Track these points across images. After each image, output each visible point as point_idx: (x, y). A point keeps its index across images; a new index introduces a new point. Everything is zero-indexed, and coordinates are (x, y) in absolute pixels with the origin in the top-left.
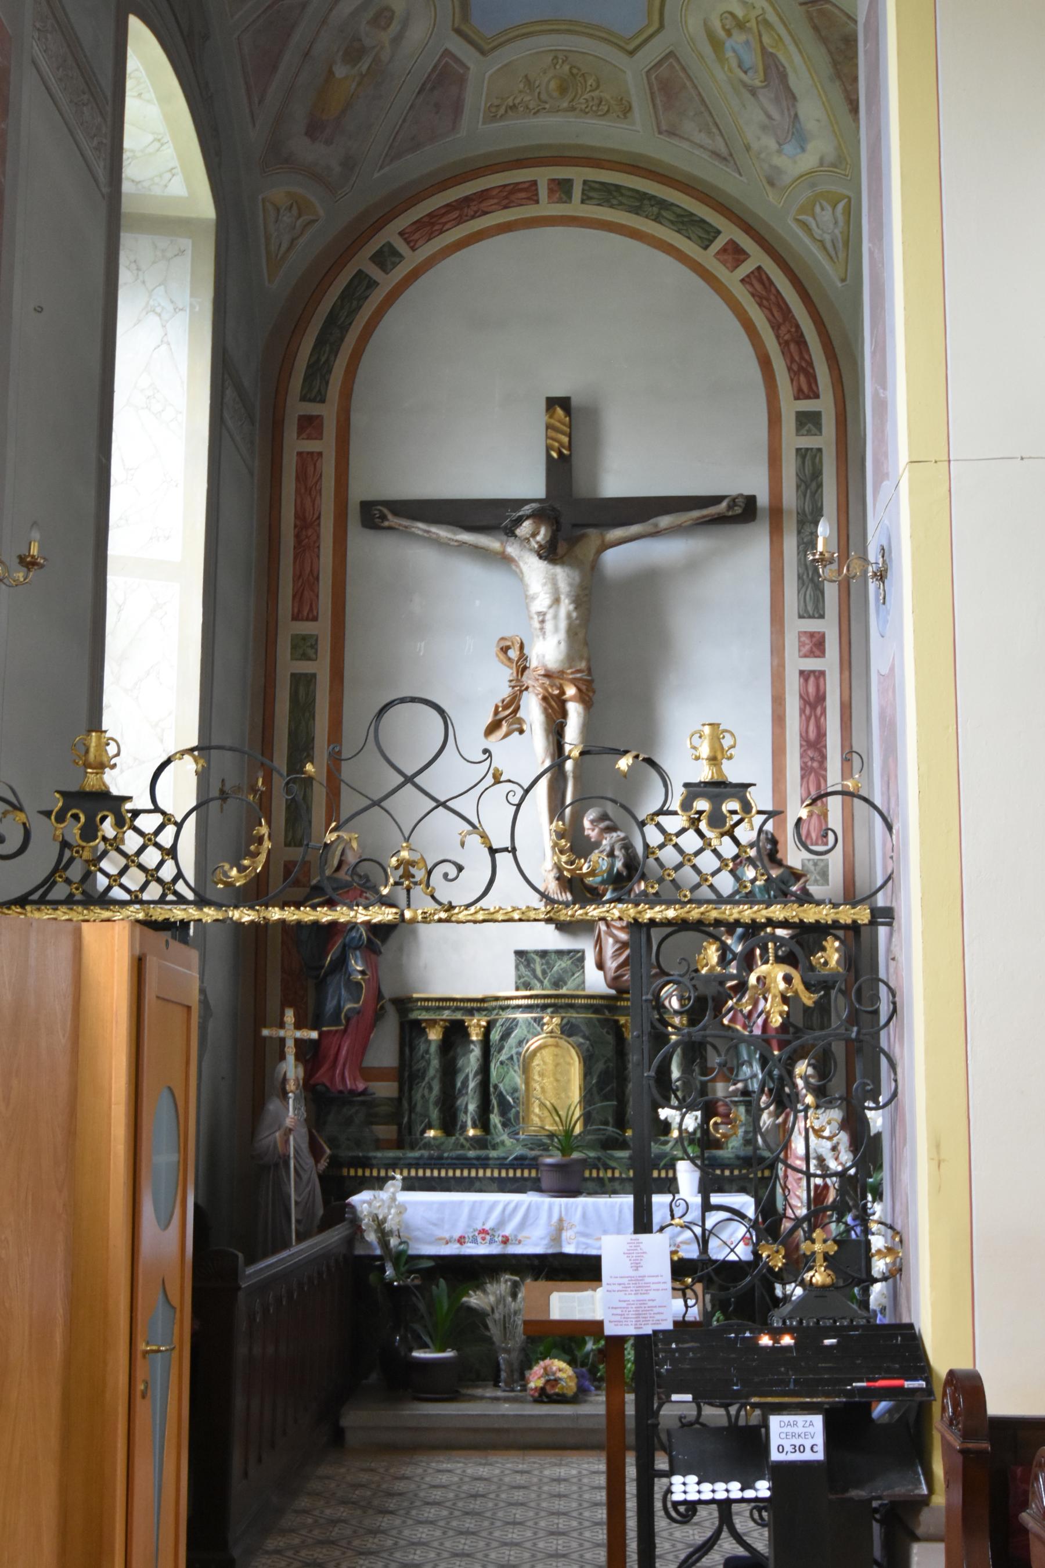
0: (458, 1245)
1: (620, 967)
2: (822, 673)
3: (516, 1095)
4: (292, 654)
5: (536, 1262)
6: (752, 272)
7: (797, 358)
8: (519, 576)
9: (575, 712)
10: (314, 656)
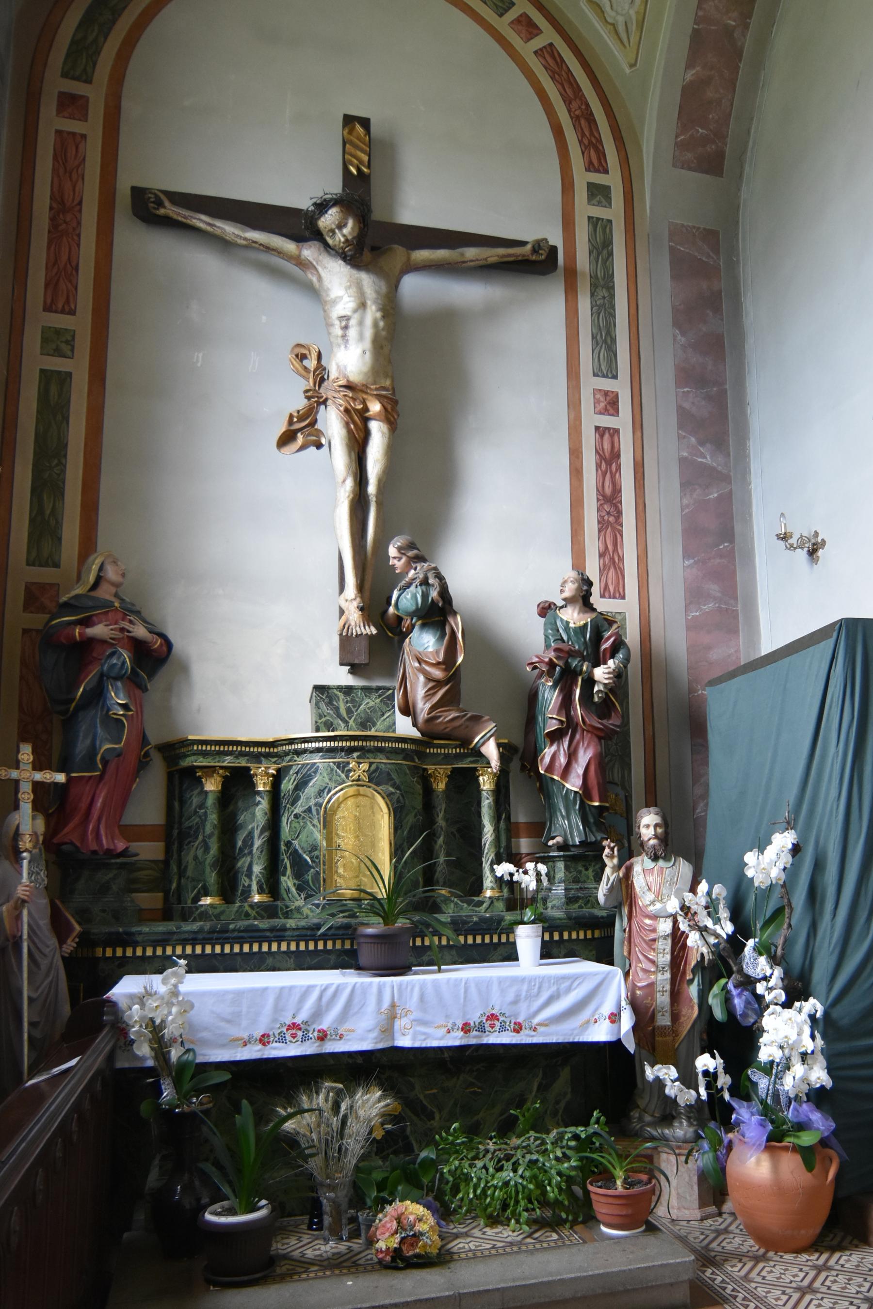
0: (260, 1046)
1: (433, 708)
2: (617, 431)
3: (316, 853)
4: (41, 347)
5: (360, 1060)
6: (545, 47)
7: (587, 134)
8: (314, 292)
9: (378, 431)
10: (69, 353)
